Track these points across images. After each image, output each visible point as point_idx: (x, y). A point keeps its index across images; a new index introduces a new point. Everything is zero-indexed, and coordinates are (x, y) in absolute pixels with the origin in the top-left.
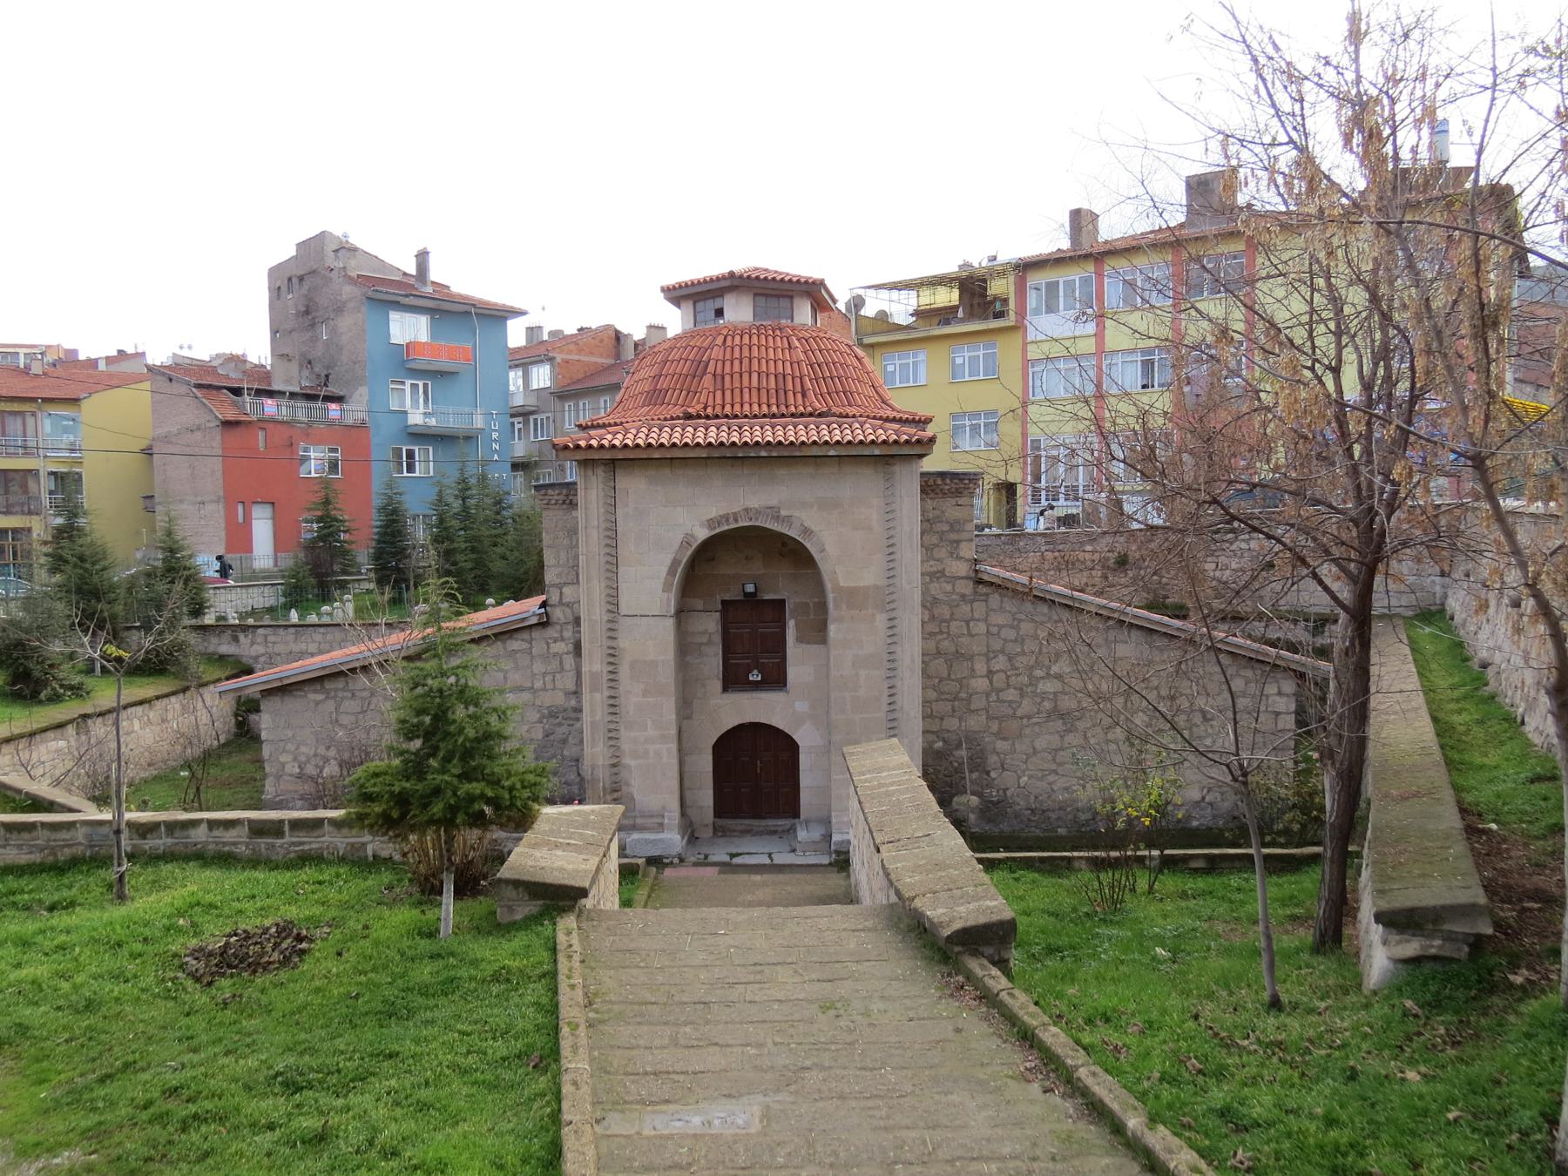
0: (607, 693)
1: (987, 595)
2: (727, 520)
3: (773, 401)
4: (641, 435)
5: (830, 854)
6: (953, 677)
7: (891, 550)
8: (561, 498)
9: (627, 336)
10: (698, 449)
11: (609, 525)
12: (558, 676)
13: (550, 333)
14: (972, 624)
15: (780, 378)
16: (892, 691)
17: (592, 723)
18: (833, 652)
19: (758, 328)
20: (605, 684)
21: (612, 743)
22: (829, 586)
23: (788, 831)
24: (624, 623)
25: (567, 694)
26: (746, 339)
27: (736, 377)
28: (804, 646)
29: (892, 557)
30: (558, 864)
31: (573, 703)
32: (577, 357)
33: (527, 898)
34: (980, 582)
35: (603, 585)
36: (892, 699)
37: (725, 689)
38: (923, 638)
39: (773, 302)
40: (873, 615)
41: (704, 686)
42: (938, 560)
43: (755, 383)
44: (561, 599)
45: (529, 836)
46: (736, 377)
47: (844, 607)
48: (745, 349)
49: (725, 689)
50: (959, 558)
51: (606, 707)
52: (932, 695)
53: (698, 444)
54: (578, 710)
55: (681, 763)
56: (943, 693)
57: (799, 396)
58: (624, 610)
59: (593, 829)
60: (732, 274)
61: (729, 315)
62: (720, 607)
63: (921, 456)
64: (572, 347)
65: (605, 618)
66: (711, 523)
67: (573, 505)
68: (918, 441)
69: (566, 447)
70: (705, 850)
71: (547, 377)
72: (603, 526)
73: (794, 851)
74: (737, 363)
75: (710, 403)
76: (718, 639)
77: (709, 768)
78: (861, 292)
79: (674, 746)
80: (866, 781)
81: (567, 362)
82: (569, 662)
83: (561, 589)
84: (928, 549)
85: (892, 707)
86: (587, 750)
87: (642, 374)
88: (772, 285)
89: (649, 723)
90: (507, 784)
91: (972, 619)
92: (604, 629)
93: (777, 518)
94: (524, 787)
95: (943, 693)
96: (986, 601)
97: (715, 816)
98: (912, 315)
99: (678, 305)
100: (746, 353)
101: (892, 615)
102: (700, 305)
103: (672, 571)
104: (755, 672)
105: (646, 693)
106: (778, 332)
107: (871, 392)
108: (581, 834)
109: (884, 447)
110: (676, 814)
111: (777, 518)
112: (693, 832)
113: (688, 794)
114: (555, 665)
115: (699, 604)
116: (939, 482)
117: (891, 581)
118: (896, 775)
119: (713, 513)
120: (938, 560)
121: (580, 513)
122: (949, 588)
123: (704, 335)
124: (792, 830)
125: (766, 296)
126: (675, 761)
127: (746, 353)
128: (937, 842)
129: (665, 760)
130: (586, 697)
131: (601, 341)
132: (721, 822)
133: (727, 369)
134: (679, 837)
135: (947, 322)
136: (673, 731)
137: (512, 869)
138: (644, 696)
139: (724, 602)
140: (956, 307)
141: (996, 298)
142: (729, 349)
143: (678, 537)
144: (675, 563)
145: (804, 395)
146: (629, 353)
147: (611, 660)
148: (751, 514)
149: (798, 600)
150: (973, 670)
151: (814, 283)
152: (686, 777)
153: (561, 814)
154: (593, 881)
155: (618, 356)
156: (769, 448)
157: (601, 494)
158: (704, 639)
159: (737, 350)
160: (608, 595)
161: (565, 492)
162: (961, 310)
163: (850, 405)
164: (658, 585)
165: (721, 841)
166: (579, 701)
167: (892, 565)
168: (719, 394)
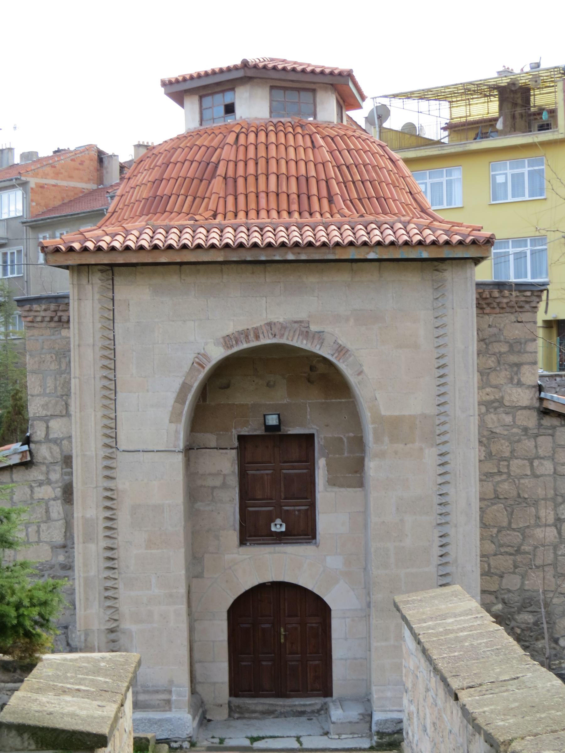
0: (103, 543)
1: (554, 428)
2: (247, 336)
3: (295, 207)
4: (145, 236)
5: (371, 737)
6: (514, 526)
7: (442, 372)
8: (49, 314)
9: (113, 157)
10: (212, 251)
11: (107, 343)
12: (43, 527)
13: (24, 156)
14: (536, 462)
15: (303, 181)
16: (444, 541)
17: (86, 579)
18: (373, 495)
19: (275, 126)
20: (101, 533)
21: (109, 603)
22: (367, 416)
23: (318, 711)
24: (122, 459)
25: (55, 548)
26: (262, 136)
27: (251, 180)
28: (336, 489)
29: (442, 381)
30: (68, 709)
31: (61, 558)
32: (53, 182)
33: (33, 747)
34: (546, 412)
35: (100, 414)
36: (444, 550)
37: (243, 542)
38: (481, 480)
39: (292, 96)
40: (421, 449)
42: (496, 387)
43: (273, 187)
44: (47, 434)
45: (31, 679)
46: (251, 180)
47: (386, 439)
48: (262, 148)
49: (243, 542)
50: (520, 384)
52: (491, 548)
53: (213, 246)
54: (68, 567)
55: (191, 630)
56: (501, 546)
57: (325, 202)
58: (123, 445)
59: (106, 676)
60: (245, 64)
61: (242, 112)
62: (236, 444)
63: (477, 261)
64: (48, 169)
66: (227, 341)
67: (64, 323)
68: (474, 242)
69: (57, 250)
70: (219, 734)
71: (20, 206)
72: (99, 344)
73: (326, 733)
74: (251, 164)
75: (221, 209)
76: (234, 481)
77: (223, 636)
78: (385, 101)
79: (183, 608)
80: (429, 628)
81: (42, 187)
82: (57, 509)
83: (47, 422)
84: (484, 373)
85: (444, 560)
86: (80, 612)
87: (140, 178)
88: (293, 77)
90: (13, 599)
91: (538, 457)
92: (100, 467)
93: (306, 334)
94: (33, 605)
95: (501, 546)
96: (552, 435)
97: (231, 695)
98: (444, 129)
99: (181, 103)
100: (262, 152)
101: (443, 449)
102: (207, 101)
103: (180, 398)
104: (278, 521)
105: (150, 544)
106: (299, 130)
107: (409, 199)
108: (92, 681)
109: (433, 248)
110: (186, 690)
111: (306, 334)
112: (204, 713)
113: (197, 666)
114: (40, 511)
115: (211, 439)
116: (496, 294)
117: (442, 409)
118: (465, 621)
119: (231, 329)
120: (496, 387)
121: (72, 332)
122: (508, 419)
123: (212, 133)
124: (324, 710)
125: (285, 89)
126: (184, 626)
127: (262, 152)
128: (528, 684)
130: (79, 548)
131: (82, 163)
132: (237, 701)
133: (241, 171)
134: (190, 717)
135: (485, 136)
136: (182, 590)
137: (14, 713)
139: (241, 438)
140: (496, 120)
141: (541, 110)
142: (242, 149)
143: (189, 357)
144: (184, 388)
145: (331, 201)
146: (113, 176)
147: (109, 504)
148: (275, 330)
149: (329, 435)
150: (538, 518)
151: (340, 74)
152: (196, 646)
153: (65, 660)
154: (113, 727)
155: (100, 180)
156: (297, 250)
157: (98, 306)
158: (218, 482)
159: (251, 149)
160: (106, 426)
161: (53, 306)
162: (500, 121)
163: (385, 213)
164: (164, 414)
165: (239, 723)
166: (70, 557)
167: (443, 390)
168: (230, 199)
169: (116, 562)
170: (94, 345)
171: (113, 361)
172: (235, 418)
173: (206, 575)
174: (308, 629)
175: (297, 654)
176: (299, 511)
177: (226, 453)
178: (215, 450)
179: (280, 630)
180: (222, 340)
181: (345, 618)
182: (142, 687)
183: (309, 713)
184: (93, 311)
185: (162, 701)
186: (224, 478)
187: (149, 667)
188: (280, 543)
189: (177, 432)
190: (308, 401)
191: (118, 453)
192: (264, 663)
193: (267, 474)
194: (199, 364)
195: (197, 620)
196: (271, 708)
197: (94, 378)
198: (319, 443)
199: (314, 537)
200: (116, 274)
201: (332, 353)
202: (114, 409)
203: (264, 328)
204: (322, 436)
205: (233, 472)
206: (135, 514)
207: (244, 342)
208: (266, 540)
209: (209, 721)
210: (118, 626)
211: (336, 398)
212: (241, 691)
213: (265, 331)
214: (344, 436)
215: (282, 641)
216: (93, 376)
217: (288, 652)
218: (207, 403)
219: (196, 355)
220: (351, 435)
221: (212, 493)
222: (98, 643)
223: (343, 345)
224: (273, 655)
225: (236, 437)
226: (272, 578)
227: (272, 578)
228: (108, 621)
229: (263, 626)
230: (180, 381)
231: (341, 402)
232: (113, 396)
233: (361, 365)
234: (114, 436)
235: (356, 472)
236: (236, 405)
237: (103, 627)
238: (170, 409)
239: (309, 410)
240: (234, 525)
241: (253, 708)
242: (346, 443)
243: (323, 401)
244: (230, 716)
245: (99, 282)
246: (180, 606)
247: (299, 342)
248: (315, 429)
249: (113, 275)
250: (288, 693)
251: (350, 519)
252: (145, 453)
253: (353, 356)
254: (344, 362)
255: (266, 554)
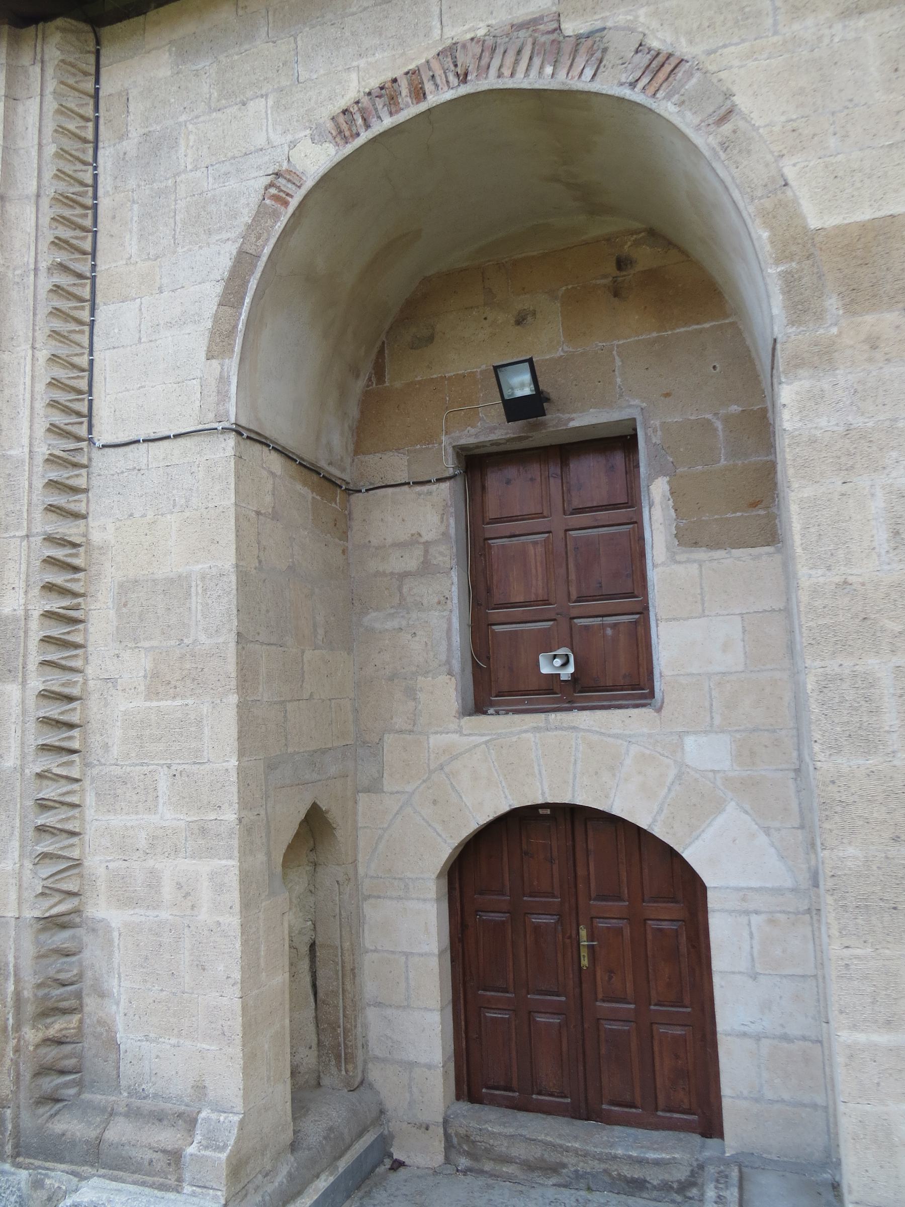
21: (47, 845)
28: (702, 554)
35: (43, 355)
41: (411, 693)
47: (833, 304)
51: (32, 726)
65: (43, 451)
72: (51, 189)
89: (163, 785)
129: (204, 915)
138: (152, 693)
147: (59, 578)
158: (411, 561)
169: (75, 733)
170: (38, 196)
171: (90, 235)
172: (447, 408)
173: (388, 784)
174: (649, 937)
175: (624, 1000)
176: (615, 626)
177: (430, 493)
178: (406, 488)
179: (578, 933)
180: (330, 125)
181: (747, 913)
182: (130, 1095)
183: (654, 1187)
184: (41, 120)
185: (159, 1155)
186: (426, 552)
187: (147, 1038)
188: (570, 709)
189: (223, 380)
190: (616, 342)
191: (96, 454)
192: (541, 1019)
193: (535, 543)
194: (275, 198)
195: (369, 897)
196: (553, 1157)
197: (36, 269)
198: (648, 439)
199: (652, 695)
200: (105, 42)
201: (631, 79)
202: (86, 343)
203: (435, 65)
204: (657, 423)
205: (443, 534)
206: (125, 605)
207: (384, 113)
208: (538, 702)
209: (398, 1165)
210: (77, 911)
211: (686, 324)
212: (488, 1088)
213: (439, 72)
214: (716, 414)
215: (585, 962)
216: (32, 266)
217: (600, 996)
218: (387, 384)
219: (267, 180)
220: (735, 408)
221: (400, 589)
222: (16, 958)
223: (666, 49)
224: (563, 999)
225: (450, 450)
226: (543, 794)
227: (543, 794)
228: (42, 894)
229: (535, 920)
230: (231, 249)
231: (701, 331)
232: (85, 315)
233: (729, 95)
234: (85, 410)
235: (754, 505)
236: (450, 378)
237: (29, 914)
238: (209, 324)
239: (618, 362)
240: (448, 662)
241: (502, 1147)
242: (720, 433)
243: (655, 334)
244: (448, 1160)
245: (59, 53)
246: (224, 862)
247: (534, 73)
248: (637, 406)
249: (98, 43)
250: (604, 1106)
251: (744, 631)
252: (151, 444)
253: (698, 75)
254: (668, 97)
255: (526, 731)
